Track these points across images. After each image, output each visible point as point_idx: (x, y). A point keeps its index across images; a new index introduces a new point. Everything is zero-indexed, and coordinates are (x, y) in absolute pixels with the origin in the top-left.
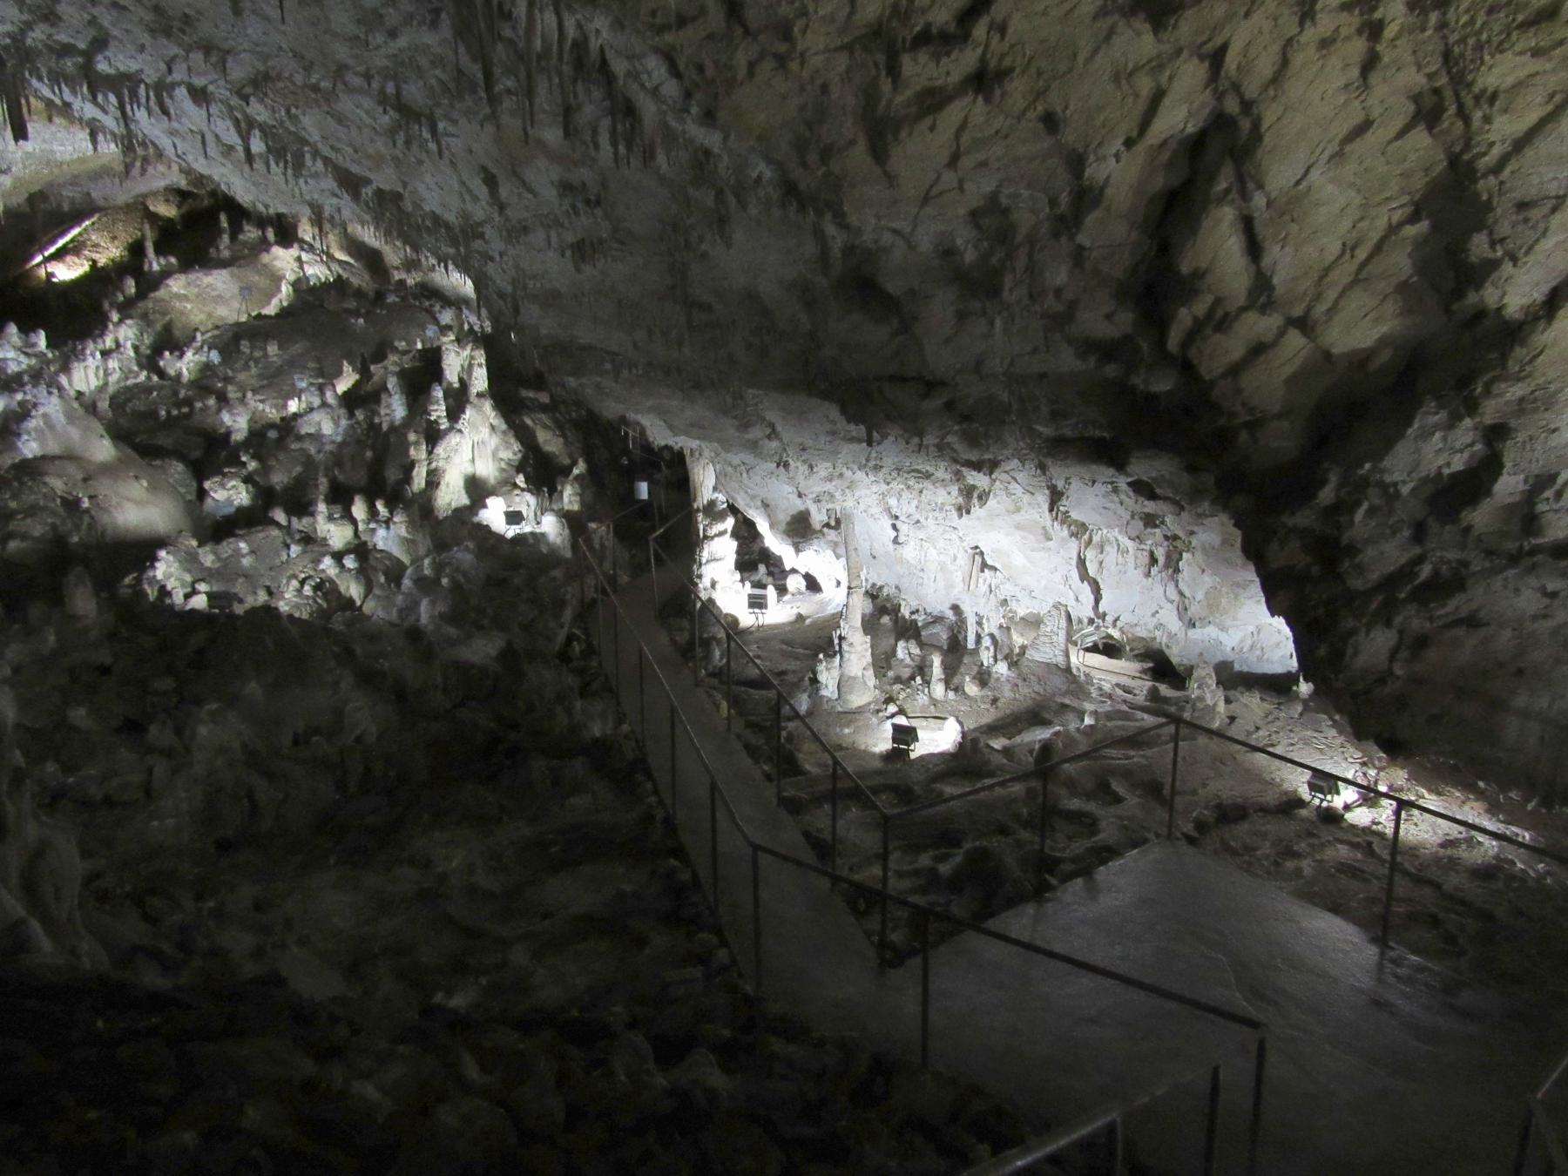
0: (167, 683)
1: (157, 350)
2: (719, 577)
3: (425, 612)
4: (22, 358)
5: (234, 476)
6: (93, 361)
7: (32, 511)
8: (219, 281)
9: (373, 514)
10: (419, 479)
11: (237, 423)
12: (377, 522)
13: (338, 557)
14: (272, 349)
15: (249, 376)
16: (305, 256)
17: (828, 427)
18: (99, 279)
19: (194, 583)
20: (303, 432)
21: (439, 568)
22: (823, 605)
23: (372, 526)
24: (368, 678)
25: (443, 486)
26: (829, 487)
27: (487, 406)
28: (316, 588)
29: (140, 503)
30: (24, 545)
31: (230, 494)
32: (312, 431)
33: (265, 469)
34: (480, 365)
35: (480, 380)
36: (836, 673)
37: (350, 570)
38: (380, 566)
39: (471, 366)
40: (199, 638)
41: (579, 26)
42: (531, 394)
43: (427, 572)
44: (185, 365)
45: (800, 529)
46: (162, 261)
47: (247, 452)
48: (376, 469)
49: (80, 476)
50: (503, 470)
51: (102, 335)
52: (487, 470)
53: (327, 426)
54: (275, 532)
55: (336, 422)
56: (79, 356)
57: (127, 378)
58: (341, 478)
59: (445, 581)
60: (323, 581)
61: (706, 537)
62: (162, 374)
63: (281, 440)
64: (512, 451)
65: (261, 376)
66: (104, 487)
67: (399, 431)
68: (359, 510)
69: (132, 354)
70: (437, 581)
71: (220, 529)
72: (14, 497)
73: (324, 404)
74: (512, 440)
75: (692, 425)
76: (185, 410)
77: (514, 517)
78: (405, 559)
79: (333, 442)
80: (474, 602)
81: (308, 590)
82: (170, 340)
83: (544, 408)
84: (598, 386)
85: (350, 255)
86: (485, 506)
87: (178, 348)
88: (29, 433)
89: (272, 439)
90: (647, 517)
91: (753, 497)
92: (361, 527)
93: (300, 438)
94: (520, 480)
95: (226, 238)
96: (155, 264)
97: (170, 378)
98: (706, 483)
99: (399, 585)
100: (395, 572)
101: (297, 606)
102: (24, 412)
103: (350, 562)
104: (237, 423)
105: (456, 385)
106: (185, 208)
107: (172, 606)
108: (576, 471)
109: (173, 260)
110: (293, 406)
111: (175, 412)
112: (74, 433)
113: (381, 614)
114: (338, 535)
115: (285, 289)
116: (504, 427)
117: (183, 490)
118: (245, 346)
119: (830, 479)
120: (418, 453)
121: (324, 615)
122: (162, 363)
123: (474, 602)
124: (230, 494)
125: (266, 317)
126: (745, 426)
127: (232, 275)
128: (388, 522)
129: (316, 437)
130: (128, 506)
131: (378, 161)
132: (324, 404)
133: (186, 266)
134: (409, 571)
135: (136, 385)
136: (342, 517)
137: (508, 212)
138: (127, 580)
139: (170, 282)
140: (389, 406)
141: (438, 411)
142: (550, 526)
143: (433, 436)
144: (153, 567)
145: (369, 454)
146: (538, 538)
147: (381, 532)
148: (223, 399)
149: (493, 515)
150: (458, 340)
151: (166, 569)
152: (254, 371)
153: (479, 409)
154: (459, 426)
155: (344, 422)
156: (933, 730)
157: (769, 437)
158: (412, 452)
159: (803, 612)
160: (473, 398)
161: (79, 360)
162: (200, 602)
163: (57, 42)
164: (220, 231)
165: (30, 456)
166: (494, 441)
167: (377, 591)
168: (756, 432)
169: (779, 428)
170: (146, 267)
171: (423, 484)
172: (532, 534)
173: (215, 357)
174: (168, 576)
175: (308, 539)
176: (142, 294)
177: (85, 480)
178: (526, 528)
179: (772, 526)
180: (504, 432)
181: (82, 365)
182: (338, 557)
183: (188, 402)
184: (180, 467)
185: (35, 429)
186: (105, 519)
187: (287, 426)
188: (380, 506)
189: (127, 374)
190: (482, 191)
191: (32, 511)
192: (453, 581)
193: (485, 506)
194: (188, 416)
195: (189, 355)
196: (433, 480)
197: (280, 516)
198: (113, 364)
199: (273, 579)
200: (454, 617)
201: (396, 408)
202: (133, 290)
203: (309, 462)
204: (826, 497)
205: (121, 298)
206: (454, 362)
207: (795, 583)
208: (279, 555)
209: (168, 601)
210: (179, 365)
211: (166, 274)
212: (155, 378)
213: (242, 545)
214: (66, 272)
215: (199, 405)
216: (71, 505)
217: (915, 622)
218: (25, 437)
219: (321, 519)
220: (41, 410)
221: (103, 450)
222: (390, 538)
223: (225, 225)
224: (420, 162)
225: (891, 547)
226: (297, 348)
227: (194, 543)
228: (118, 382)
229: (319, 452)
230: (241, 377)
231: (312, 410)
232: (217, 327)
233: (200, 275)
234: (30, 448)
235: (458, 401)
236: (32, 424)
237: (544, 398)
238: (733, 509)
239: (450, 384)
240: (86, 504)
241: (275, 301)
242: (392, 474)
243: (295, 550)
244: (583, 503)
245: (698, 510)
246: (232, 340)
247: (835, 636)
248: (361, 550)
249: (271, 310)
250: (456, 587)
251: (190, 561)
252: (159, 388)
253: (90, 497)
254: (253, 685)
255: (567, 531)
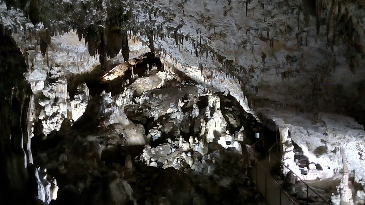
0: (148, 189)
1: (134, 96)
2: (289, 162)
3: (210, 170)
4: (111, 100)
5: (157, 129)
6: (121, 99)
7: (113, 138)
8: (147, 80)
9: (194, 141)
10: (203, 132)
11: (156, 115)
12: (195, 143)
13: (186, 153)
14: (160, 96)
15: (155, 103)
16: (167, 73)
17: (347, 124)
18: (120, 80)
19: (150, 158)
20: (172, 118)
21: (212, 157)
22: (325, 175)
23: (194, 144)
24: (199, 190)
25: (209, 133)
26: (339, 141)
27: (220, 112)
28: (181, 161)
29: (135, 136)
30: (111, 146)
31: (156, 134)
32: (175, 118)
33: (163, 128)
34: (218, 102)
35: (218, 106)
36: (339, 200)
37: (189, 157)
38: (196, 156)
39: (216, 101)
40: (155, 176)
41: (346, 9)
42: (227, 108)
43: (209, 158)
44: (140, 100)
45: (320, 151)
46: (135, 75)
47: (159, 123)
48: (192, 130)
49: (122, 129)
50: (223, 129)
51: (123, 93)
52: (219, 129)
53: (179, 116)
54: (169, 145)
55: (181, 115)
56: (118, 98)
57: (128, 103)
58: (183, 130)
59: (214, 161)
60: (182, 160)
61: (286, 152)
62: (135, 102)
63: (166, 120)
64: (225, 124)
65: (157, 103)
66: (127, 131)
67: (198, 118)
68: (191, 140)
69: (129, 97)
70: (211, 161)
71: (154, 143)
72: (110, 134)
73: (178, 111)
74: (225, 121)
75: (294, 122)
76: (141, 111)
77: (228, 143)
78: (203, 154)
79: (180, 121)
80: (221, 168)
81: (179, 162)
82: (136, 94)
83: (231, 112)
84: (267, 110)
85: (175, 73)
86: (219, 139)
87: (139, 96)
88: (112, 118)
89: (165, 119)
90: (266, 143)
91: (303, 141)
92: (191, 145)
93: (171, 119)
94: (228, 132)
95: (148, 70)
96: (133, 76)
97: (137, 103)
98: (285, 137)
99: (201, 162)
100: (200, 158)
101: (176, 166)
102: (111, 113)
103: (189, 155)
104: (156, 115)
105: (212, 107)
106: (137, 63)
107: (147, 165)
108: (241, 130)
109: (137, 75)
110: (169, 111)
111: (139, 112)
112: (121, 118)
113: (197, 169)
114: (186, 147)
115: (163, 82)
116: (223, 117)
117: (142, 132)
118: (154, 96)
119: (340, 138)
120: (203, 125)
121: (182, 169)
122: (135, 100)
123: (221, 168)
124: (156, 134)
125: (158, 88)
126: (315, 123)
127: (150, 78)
128: (198, 143)
129: (175, 119)
130: (133, 136)
131: (230, 52)
132: (178, 111)
133: (140, 76)
134: (203, 157)
135: (130, 105)
136: (187, 142)
137: (266, 65)
138: (136, 158)
139: (137, 80)
140: (195, 112)
141: (208, 113)
142: (236, 145)
143: (207, 120)
144: (142, 154)
145: (190, 124)
146: (234, 148)
147: (197, 146)
148: (150, 108)
149: (222, 142)
150: (213, 95)
151: (145, 155)
152: (156, 102)
153: (218, 113)
154: (213, 117)
155: (182, 116)
156: (31, 105)
157: (322, 126)
158: (202, 124)
159: (319, 177)
160: (216, 110)
161: (118, 99)
162: (154, 164)
163: (169, 27)
164: (147, 68)
165: (112, 124)
166: (221, 121)
167: (196, 163)
168: (318, 125)
169: (326, 124)
170: (131, 77)
171: (204, 133)
172: (232, 147)
173: (148, 98)
174: (145, 156)
175: (176, 147)
176: (130, 83)
177: (123, 130)
178: (231, 146)
179: (309, 150)
180: (223, 119)
181: (118, 100)
182: (186, 153)
183: (142, 109)
184: (142, 126)
185: (113, 117)
186: (128, 140)
187: (168, 116)
188: (196, 139)
189: (128, 102)
190: (260, 59)
191: (113, 138)
192: (216, 161)
193: (219, 139)
194: (142, 113)
195: (141, 98)
196: (206, 133)
197: (169, 140)
198: (125, 100)
199: (169, 158)
200: (216, 172)
201: (196, 112)
202: (129, 82)
203: (174, 126)
204: (337, 144)
205: (126, 84)
206: (211, 101)
207: (312, 166)
208: (169, 151)
209: (145, 163)
210: (139, 100)
211: (136, 79)
212: (134, 103)
213: (161, 148)
214: (112, 77)
215: (144, 110)
216: (121, 136)
217: (360, 184)
218: (111, 119)
219: (180, 142)
220: (115, 112)
221: (127, 122)
222: (199, 148)
223: (148, 67)
224: (242, 52)
225: (359, 160)
226: (166, 96)
227: (150, 147)
228: (126, 104)
229: (176, 123)
230: (153, 103)
231: (175, 112)
232: (148, 91)
233: (143, 78)
234: (112, 122)
235: (213, 110)
236: (112, 116)
237: (231, 109)
238: (294, 143)
239: (211, 106)
240: (124, 136)
241: (160, 85)
242: (196, 130)
243: (174, 150)
244: (244, 139)
245: (283, 144)
246: (152, 94)
247: (338, 187)
248: (191, 151)
249: (159, 86)
250: (216, 162)
251: (149, 152)
252: (135, 106)
253: (125, 134)
254: (170, 190)
255: (241, 147)
